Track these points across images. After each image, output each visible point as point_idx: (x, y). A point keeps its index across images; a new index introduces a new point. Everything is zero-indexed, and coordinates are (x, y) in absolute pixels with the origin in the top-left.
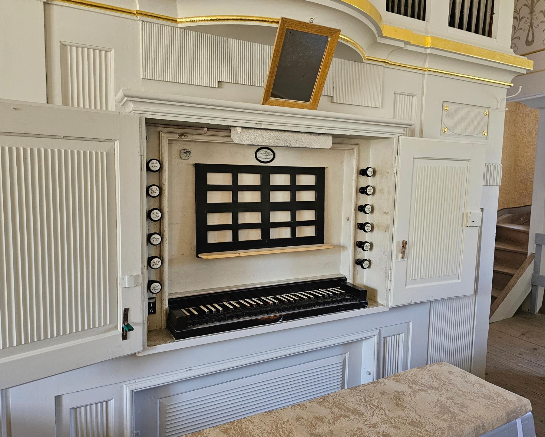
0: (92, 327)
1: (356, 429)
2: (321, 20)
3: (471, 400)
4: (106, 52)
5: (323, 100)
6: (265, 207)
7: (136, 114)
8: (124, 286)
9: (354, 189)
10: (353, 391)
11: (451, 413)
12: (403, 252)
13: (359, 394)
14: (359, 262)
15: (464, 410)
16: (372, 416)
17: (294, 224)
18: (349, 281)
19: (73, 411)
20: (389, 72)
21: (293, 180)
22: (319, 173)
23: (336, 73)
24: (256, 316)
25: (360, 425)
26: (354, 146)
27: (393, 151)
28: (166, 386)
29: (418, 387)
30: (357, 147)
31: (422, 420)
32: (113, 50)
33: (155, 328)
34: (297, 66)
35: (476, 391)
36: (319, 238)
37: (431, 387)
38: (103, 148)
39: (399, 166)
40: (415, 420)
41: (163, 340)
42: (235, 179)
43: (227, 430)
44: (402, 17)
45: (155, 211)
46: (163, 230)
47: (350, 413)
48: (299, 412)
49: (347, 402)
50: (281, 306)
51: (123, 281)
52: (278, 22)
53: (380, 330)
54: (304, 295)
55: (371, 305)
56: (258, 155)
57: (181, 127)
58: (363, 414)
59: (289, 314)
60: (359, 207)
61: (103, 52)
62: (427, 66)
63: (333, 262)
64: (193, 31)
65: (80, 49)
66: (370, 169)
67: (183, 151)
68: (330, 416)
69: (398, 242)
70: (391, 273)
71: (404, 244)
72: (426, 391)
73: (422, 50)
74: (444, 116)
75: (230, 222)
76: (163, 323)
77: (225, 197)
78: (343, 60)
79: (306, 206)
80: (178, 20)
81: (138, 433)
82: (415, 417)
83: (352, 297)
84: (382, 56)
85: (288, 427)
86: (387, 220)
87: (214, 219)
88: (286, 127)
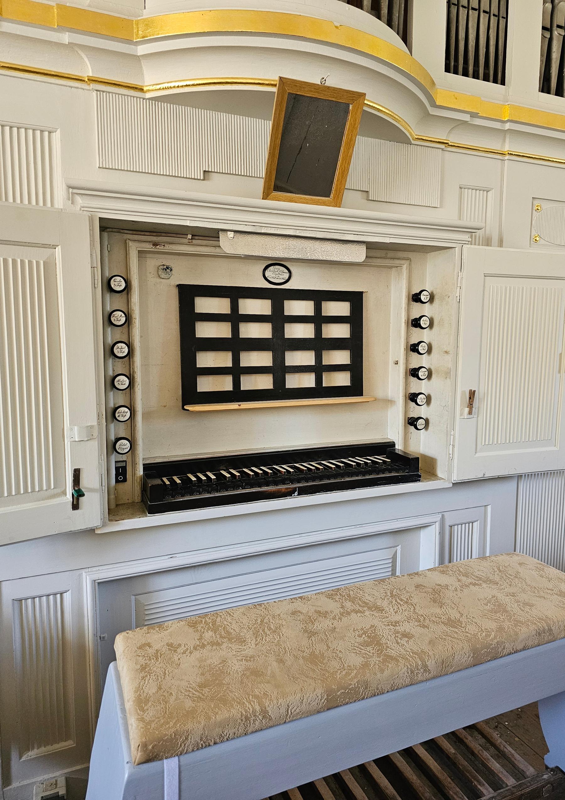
0: (30, 491)
1: (368, 627)
2: (338, 80)
3: (540, 597)
4: (50, 132)
5: (348, 196)
6: (279, 345)
7: (85, 212)
8: (73, 440)
9: (403, 321)
10: (380, 583)
11: (507, 612)
13: (386, 587)
14: (412, 422)
15: (527, 609)
16: (396, 613)
17: (319, 369)
18: (399, 447)
19: (17, 604)
20: (452, 158)
21: (318, 309)
22: (356, 299)
23: (363, 156)
24: (260, 487)
25: (376, 622)
26: (402, 262)
27: (455, 265)
29: (470, 580)
30: (408, 262)
31: (463, 619)
32: (59, 131)
33: (127, 501)
34: (309, 144)
35: (551, 587)
36: (356, 389)
37: (488, 581)
38: (38, 256)
39: (463, 287)
40: (453, 618)
41: (132, 514)
42: (235, 307)
43: (196, 623)
44: (470, 81)
45: (120, 345)
46: (134, 372)
47: (365, 609)
48: (298, 605)
49: (366, 595)
50: (299, 476)
51: (72, 433)
52: (275, 85)
53: (443, 516)
54: (332, 464)
55: (425, 479)
56: (267, 274)
57: (154, 234)
58: (383, 610)
59: (307, 486)
60: (412, 345)
61: (46, 134)
62: (507, 148)
63: (377, 422)
64: (167, 103)
65: (15, 130)
66: (424, 293)
67: (162, 267)
68: (337, 611)
69: (463, 393)
70: (454, 435)
71: (472, 394)
72: (480, 585)
73: (497, 125)
74: (534, 218)
76: (136, 495)
77: (222, 330)
78: (382, 141)
79: (337, 344)
80: (145, 89)
81: (104, 638)
82: (454, 614)
83: (395, 466)
84: (439, 133)
85: (277, 621)
86: (448, 362)
87: (205, 360)
88: (298, 231)
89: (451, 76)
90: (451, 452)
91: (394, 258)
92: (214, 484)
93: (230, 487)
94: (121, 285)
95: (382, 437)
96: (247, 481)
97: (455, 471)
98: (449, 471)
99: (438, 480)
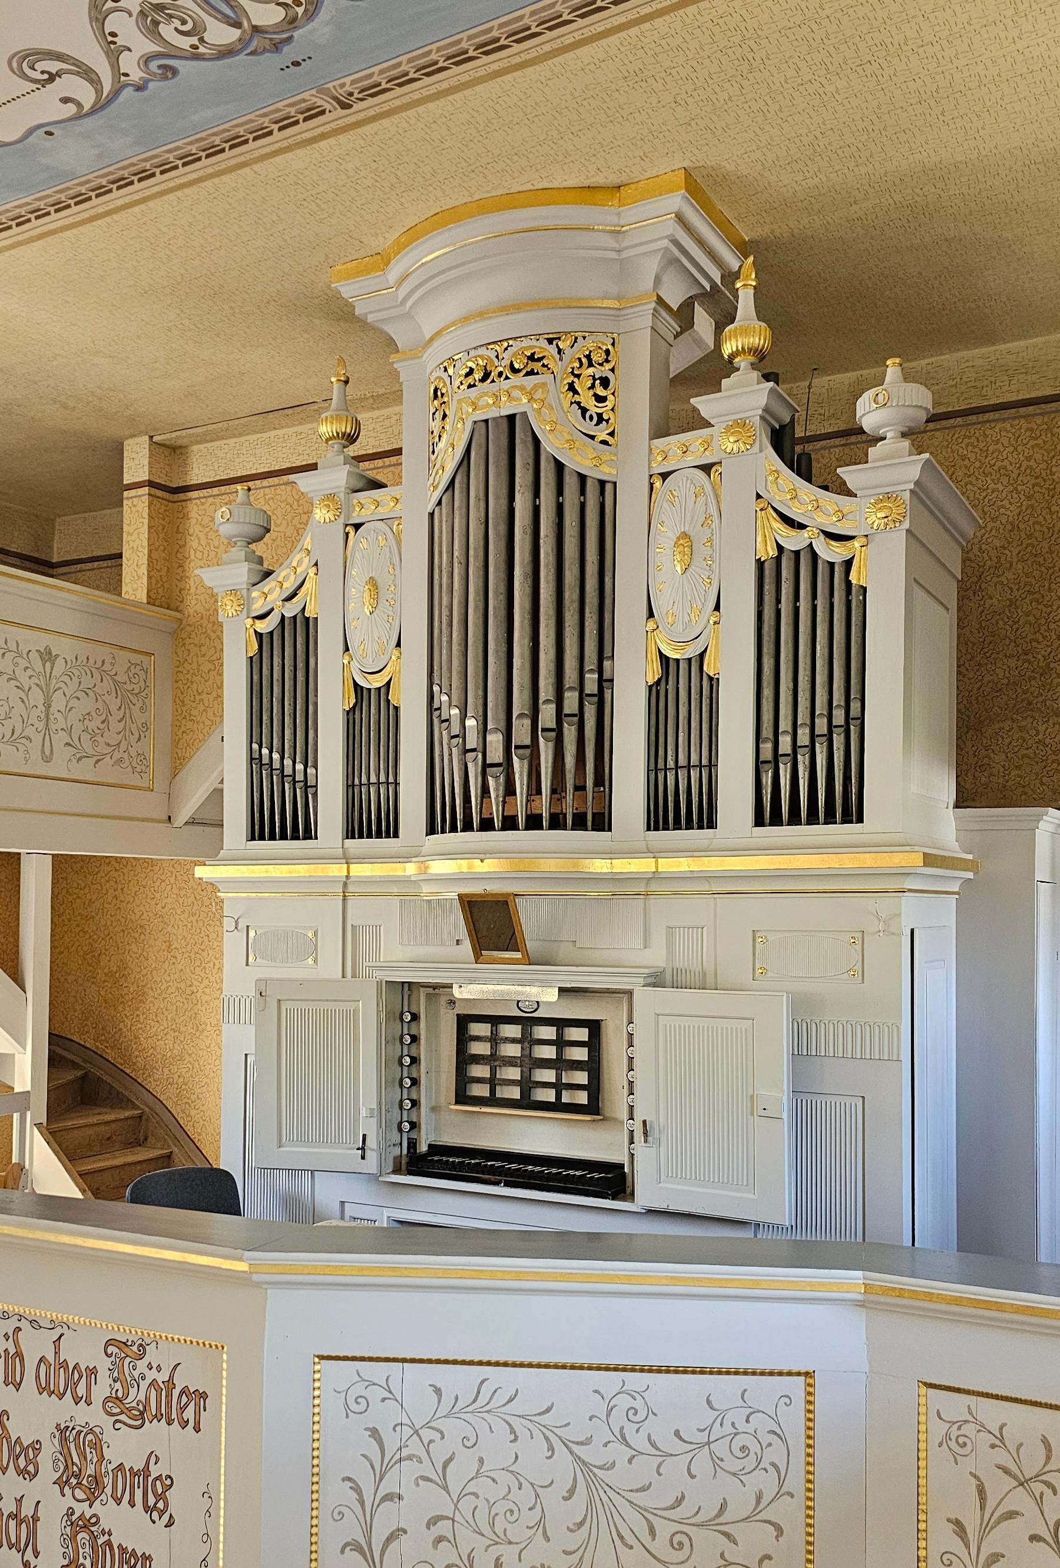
17: (559, 1087)
22: (594, 1027)
28: (151, 863)
38: (351, 1006)
50: (500, 1171)
79: (577, 1065)
89: (652, 834)
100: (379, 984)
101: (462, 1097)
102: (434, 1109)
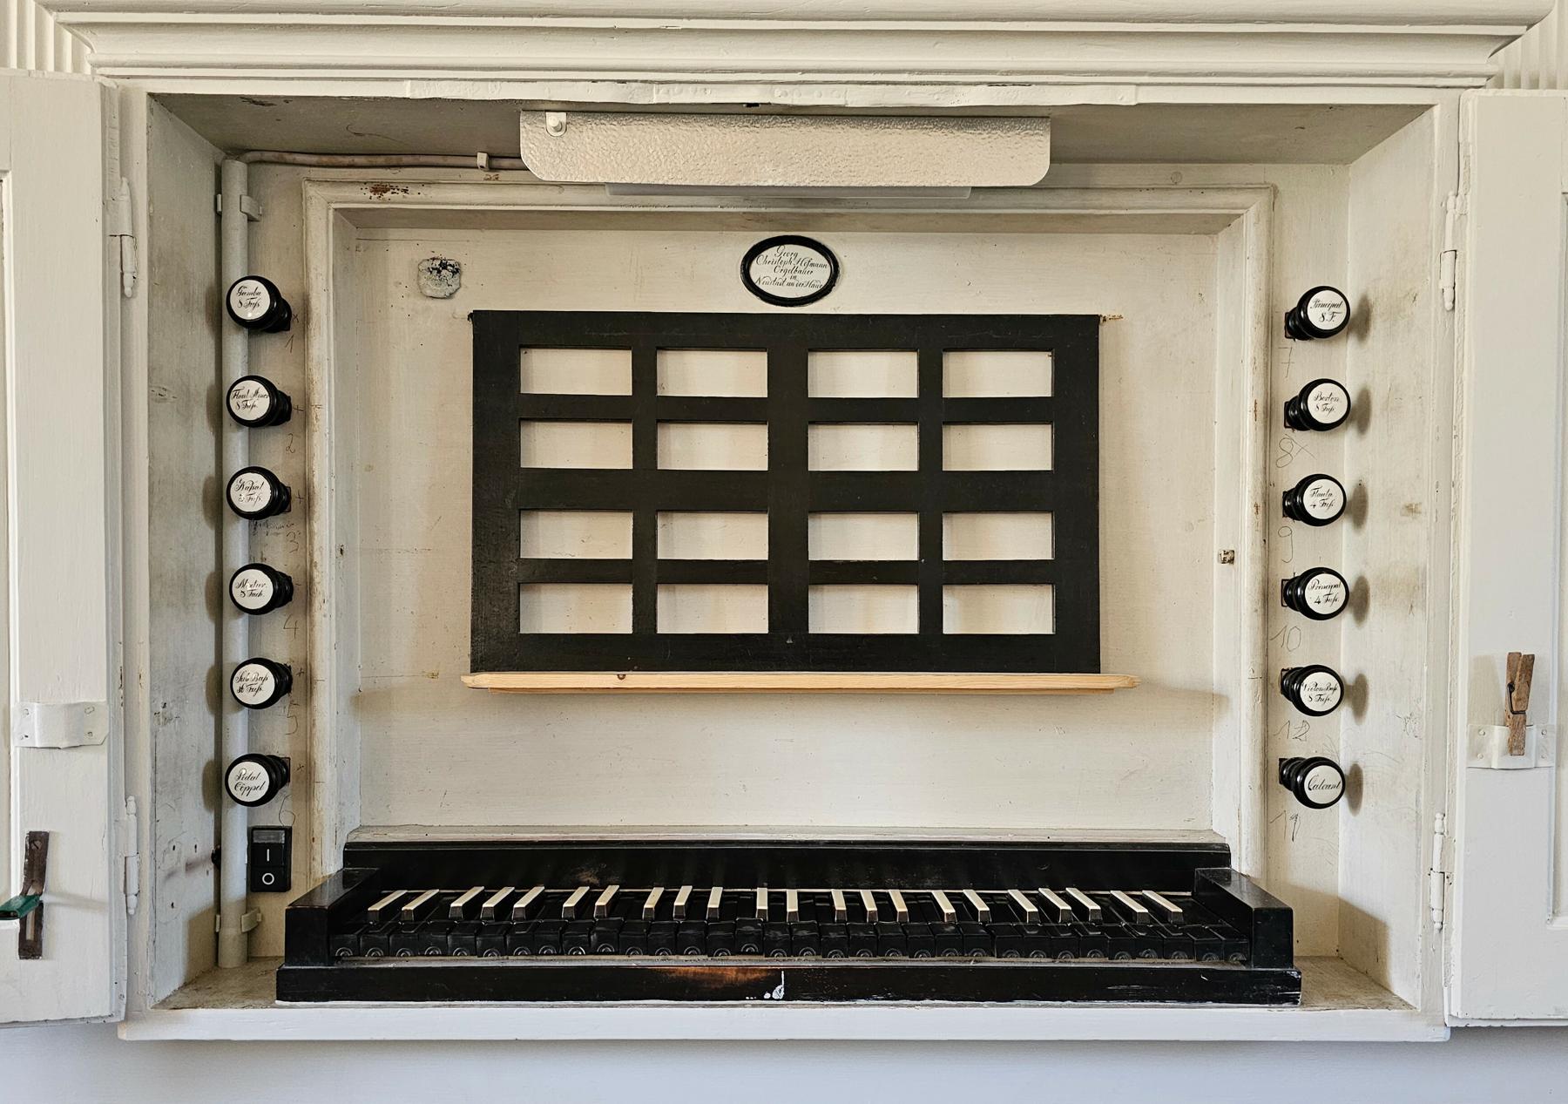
6: (791, 493)
9: (1250, 405)
12: (1517, 715)
14: (1292, 775)
21: (930, 376)
22: (1073, 342)
36: (1074, 645)
56: (761, 271)
59: (822, 969)
69: (1481, 665)
71: (1522, 669)
75: (624, 550)
83: (1194, 928)
88: (778, 90)
90: (1435, 902)
91: (1203, 189)
92: (1064, 929)
93: (548, 942)
94: (256, 305)
95: (1189, 826)
96: (625, 925)
97: (1456, 980)
98: (1442, 971)
99: (1387, 1006)
100: (114, 106)
101: (501, 644)
102: (363, 702)
